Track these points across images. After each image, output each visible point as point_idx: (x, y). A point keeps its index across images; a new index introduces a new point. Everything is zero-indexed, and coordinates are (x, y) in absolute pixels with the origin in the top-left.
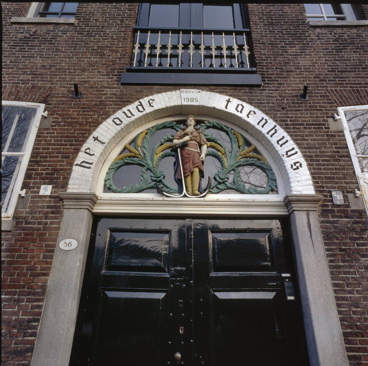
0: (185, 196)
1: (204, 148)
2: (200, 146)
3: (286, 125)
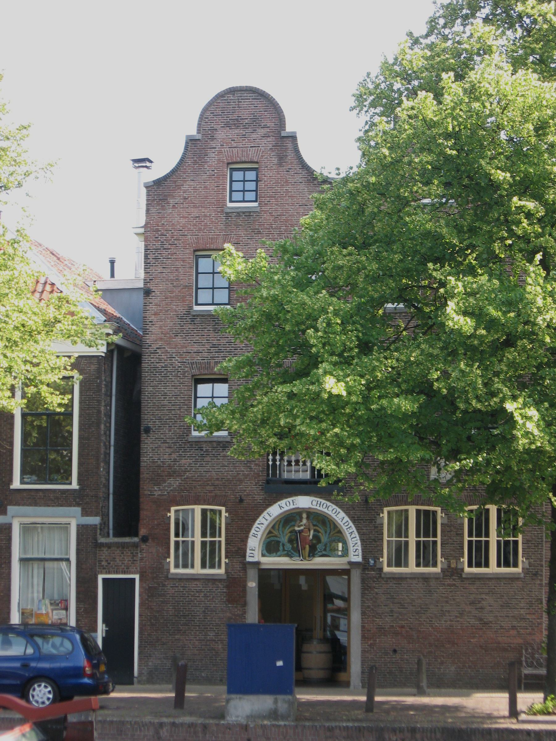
0: (302, 560)
1: (312, 532)
2: (310, 530)
3: (355, 520)
